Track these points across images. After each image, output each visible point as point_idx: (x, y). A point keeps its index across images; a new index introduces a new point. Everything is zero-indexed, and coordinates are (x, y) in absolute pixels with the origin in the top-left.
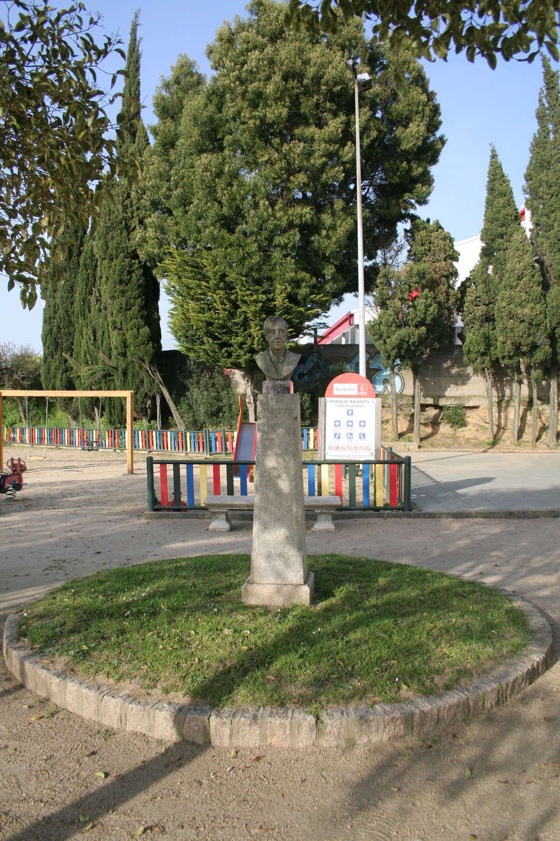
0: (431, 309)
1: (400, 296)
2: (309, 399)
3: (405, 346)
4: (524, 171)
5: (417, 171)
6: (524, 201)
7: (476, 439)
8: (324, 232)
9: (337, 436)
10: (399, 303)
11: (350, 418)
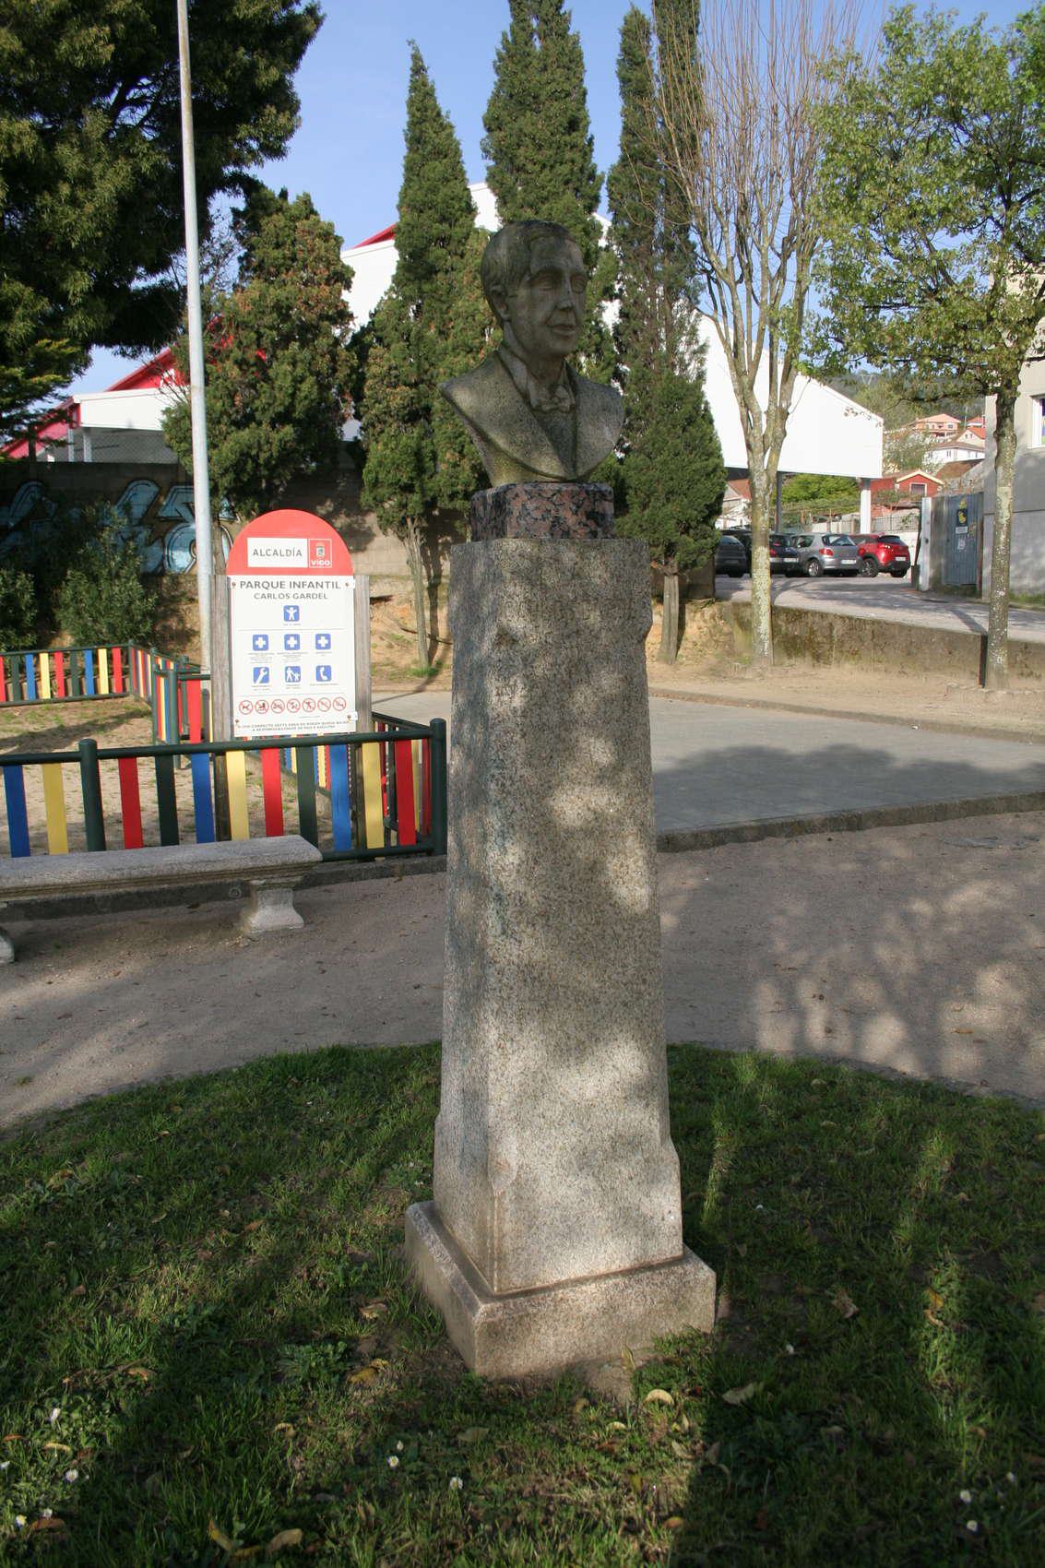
0: (305, 387)
1: (237, 354)
2: (30, 585)
3: (250, 466)
4: (483, 109)
5: (267, 76)
6: (485, 174)
7: (392, 664)
8: (65, 189)
9: (261, 675)
10: (235, 372)
11: (292, 628)
